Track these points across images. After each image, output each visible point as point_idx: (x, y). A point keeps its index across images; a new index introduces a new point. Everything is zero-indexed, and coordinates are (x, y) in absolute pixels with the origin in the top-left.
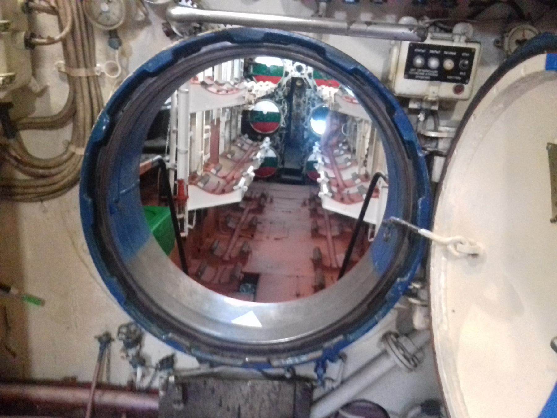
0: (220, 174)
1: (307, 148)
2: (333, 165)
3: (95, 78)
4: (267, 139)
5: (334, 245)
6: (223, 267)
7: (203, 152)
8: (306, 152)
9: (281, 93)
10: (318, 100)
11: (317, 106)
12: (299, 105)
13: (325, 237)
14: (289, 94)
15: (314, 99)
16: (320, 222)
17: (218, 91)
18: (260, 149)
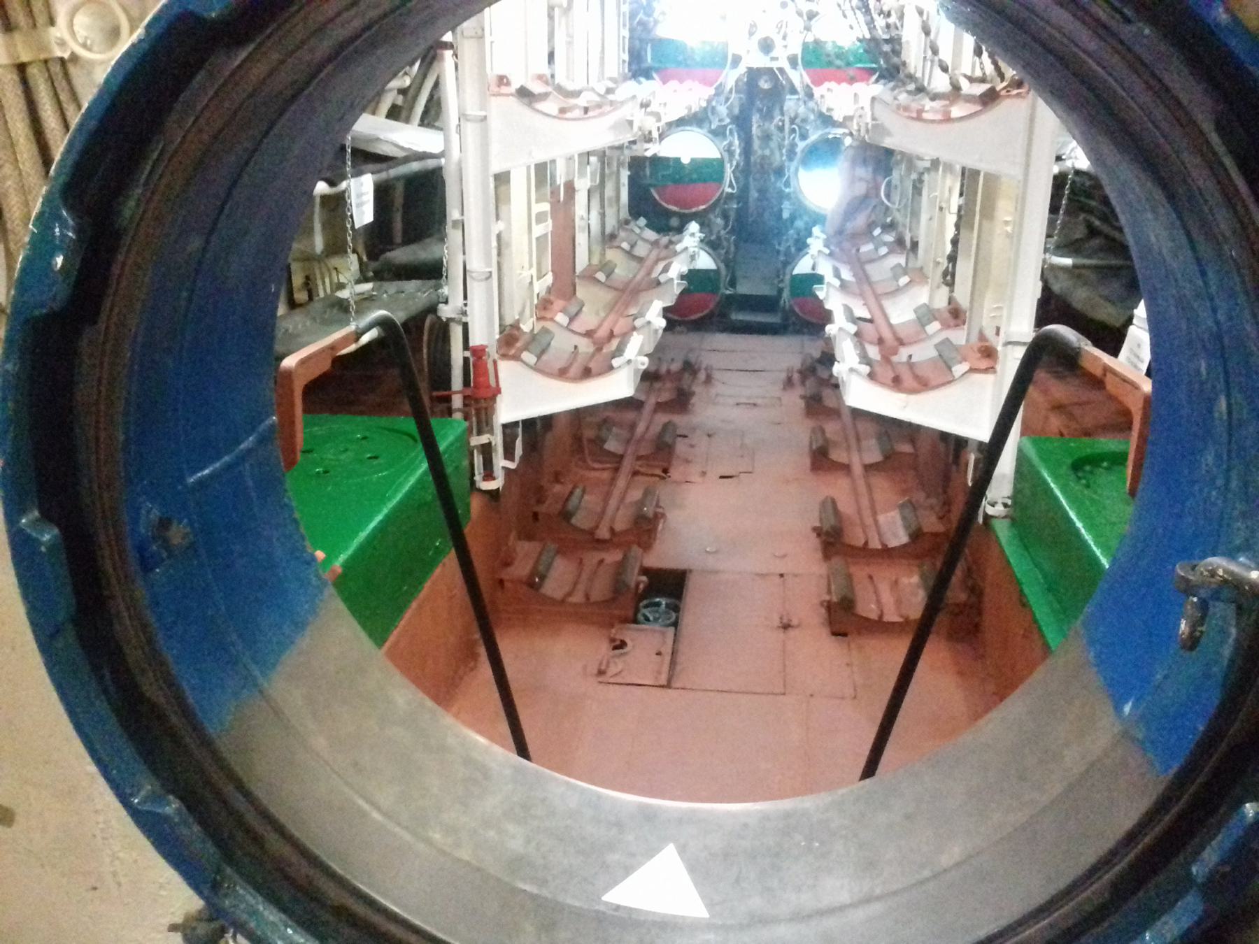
0: (579, 326)
1: (791, 243)
2: (863, 285)
3: (56, 69)
4: (694, 227)
5: (869, 488)
6: (598, 556)
7: (534, 271)
8: (787, 253)
9: (723, 110)
10: (815, 121)
11: (814, 136)
12: (767, 137)
13: (846, 468)
14: (741, 111)
15: (804, 120)
16: (831, 428)
17: (563, 111)
18: (676, 254)
